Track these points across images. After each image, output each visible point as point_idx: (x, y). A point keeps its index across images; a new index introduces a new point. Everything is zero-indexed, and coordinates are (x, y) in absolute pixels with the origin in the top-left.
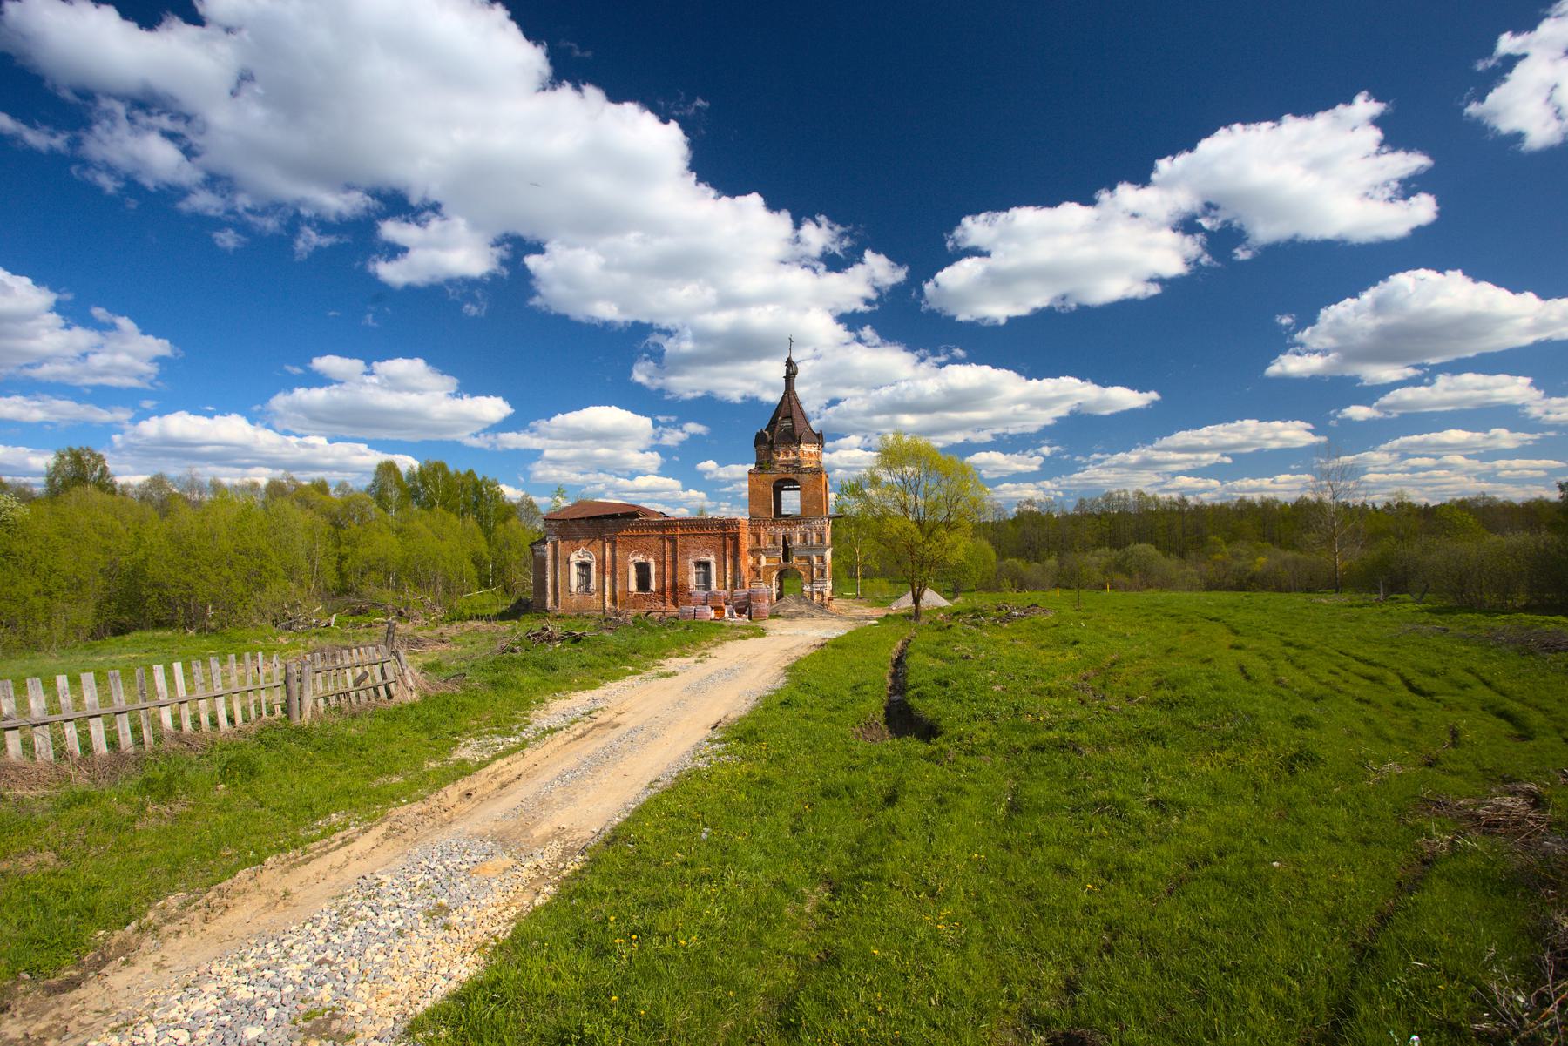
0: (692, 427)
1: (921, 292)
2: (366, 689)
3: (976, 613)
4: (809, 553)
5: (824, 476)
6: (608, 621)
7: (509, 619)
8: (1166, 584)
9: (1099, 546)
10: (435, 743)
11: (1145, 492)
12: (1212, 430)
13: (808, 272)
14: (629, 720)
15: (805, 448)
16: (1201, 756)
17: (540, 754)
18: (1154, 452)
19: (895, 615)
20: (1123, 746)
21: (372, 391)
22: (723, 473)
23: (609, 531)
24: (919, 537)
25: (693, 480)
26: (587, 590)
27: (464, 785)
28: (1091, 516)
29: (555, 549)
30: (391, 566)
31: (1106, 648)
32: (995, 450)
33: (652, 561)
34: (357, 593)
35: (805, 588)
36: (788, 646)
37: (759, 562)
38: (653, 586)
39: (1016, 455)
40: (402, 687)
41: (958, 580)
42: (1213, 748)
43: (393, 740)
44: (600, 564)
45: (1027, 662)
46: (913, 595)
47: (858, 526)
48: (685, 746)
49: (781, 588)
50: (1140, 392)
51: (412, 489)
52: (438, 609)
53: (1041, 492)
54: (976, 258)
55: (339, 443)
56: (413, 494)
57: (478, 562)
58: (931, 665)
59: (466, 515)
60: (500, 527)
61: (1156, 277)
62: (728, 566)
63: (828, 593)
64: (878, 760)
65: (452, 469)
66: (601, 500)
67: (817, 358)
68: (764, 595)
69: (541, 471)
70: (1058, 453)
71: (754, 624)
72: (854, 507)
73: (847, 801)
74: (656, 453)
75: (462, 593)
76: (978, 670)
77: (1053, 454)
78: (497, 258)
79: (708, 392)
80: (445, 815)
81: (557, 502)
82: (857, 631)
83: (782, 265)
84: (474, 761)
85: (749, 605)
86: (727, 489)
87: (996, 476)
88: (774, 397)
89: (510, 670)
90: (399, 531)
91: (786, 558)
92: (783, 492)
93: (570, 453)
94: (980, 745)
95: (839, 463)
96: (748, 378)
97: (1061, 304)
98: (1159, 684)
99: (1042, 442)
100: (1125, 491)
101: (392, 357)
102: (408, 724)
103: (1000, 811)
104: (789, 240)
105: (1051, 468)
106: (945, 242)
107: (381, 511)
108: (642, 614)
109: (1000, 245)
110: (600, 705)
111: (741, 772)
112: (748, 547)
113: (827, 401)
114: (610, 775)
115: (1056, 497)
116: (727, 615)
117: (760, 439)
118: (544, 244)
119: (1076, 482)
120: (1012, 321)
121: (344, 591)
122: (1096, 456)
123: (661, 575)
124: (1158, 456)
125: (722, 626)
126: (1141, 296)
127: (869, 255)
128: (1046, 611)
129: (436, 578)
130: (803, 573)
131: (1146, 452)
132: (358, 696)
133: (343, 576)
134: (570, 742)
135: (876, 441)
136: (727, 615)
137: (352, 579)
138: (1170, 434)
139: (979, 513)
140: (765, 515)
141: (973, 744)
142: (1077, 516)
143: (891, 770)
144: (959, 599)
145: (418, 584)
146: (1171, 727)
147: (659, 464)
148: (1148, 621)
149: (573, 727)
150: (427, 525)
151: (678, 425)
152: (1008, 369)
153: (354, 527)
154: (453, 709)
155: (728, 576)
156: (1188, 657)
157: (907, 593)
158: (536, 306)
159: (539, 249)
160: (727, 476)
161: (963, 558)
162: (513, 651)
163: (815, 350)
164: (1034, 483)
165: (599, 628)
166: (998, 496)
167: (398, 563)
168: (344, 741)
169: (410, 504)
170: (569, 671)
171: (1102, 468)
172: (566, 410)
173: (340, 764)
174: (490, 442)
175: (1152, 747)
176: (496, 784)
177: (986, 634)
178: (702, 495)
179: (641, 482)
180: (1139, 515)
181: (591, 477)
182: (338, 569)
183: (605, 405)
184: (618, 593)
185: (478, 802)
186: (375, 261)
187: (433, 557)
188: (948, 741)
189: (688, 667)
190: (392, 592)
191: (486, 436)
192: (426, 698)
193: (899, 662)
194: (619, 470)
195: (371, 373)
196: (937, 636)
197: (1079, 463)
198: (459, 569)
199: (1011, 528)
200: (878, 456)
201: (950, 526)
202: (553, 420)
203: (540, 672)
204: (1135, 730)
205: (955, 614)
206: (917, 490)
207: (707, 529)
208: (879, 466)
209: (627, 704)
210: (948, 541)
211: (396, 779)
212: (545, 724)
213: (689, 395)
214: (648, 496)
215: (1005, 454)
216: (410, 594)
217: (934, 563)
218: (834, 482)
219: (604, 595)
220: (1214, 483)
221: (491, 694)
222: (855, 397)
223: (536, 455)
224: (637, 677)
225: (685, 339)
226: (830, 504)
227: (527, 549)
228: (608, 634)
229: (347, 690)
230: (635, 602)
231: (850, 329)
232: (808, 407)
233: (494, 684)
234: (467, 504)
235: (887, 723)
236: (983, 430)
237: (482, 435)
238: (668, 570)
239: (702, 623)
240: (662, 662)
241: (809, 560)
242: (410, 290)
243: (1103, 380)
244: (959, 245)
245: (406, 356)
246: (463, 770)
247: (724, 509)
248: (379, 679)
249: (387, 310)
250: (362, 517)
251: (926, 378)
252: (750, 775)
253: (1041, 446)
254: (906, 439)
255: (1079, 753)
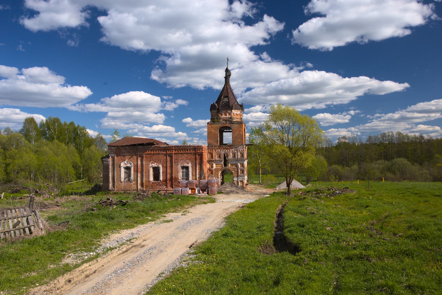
0: (180, 102)
1: (291, 35)
2: (19, 229)
3: (318, 192)
4: (236, 162)
5: (244, 125)
6: (139, 195)
7: (91, 195)
8: (413, 178)
9: (379, 159)
10: (53, 255)
11: (402, 132)
12: (436, 102)
13: (236, 26)
14: (149, 244)
15: (235, 112)
16: (431, 264)
17: (105, 260)
18: (407, 113)
19: (278, 192)
20: (391, 258)
21: (22, 83)
22: (195, 124)
23: (140, 152)
24: (289, 155)
25: (180, 127)
26: (129, 180)
27: (67, 276)
28: (375, 144)
29: (113, 160)
30: (32, 168)
31: (383, 209)
32: (327, 112)
33: (161, 166)
34: (15, 182)
35: (234, 179)
36: (226, 207)
37: (212, 167)
38: (161, 178)
39: (337, 115)
40: (37, 228)
41: (309, 176)
42: (438, 260)
43: (33, 254)
44: (136, 167)
45: (343, 216)
46: (287, 183)
47: (260, 149)
48: (177, 256)
49: (223, 179)
50: (400, 83)
51: (42, 131)
52: (55, 190)
53: (350, 133)
54: (318, 18)
55: (5, 108)
56: (43, 134)
57: (75, 167)
58: (295, 217)
59: (69, 143)
60: (87, 150)
61: (408, 26)
62: (197, 169)
63: (245, 182)
64: (270, 263)
65: (62, 122)
66: (136, 137)
67: (241, 68)
68: (214, 182)
69: (106, 123)
70: (358, 114)
71: (210, 197)
72: (258, 140)
73: (255, 283)
74: (162, 114)
75: (67, 182)
76: (319, 220)
77: (356, 115)
78: (84, 17)
79: (187, 84)
80: (58, 291)
81: (115, 137)
82: (260, 200)
83: (223, 22)
84: (72, 264)
85: (207, 187)
86: (197, 132)
87: (327, 125)
88: (219, 87)
89: (91, 219)
90: (36, 152)
91: (225, 164)
92: (224, 133)
93: (121, 114)
94: (320, 256)
95: (251, 119)
96: (207, 78)
97: (360, 40)
98: (409, 228)
99: (350, 108)
100: (392, 132)
101: (32, 66)
102: (40, 246)
103: (331, 289)
104: (227, 10)
105: (354, 122)
106: (303, 10)
107: (27, 142)
108: (156, 192)
109: (331, 11)
110: (135, 236)
111: (204, 269)
112: (207, 159)
113: (245, 89)
114: (139, 271)
115: (357, 135)
116: (197, 192)
117: (213, 107)
118: (107, 11)
119: (367, 128)
120: (335, 48)
121: (8, 181)
122: (378, 115)
123: (165, 173)
124: (409, 115)
125: (194, 198)
126: (401, 36)
127: (266, 17)
128: (352, 191)
129: (54, 175)
130: (234, 172)
131: (403, 113)
132: (15, 233)
133: (7, 174)
134: (120, 254)
135: (269, 108)
136: (197, 192)
137: (12, 175)
138: (415, 104)
139: (319, 143)
140: (215, 144)
141: (317, 256)
142: (368, 144)
143: (276, 268)
144: (309, 185)
145: (46, 178)
146: (416, 249)
147: (164, 119)
148: (403, 196)
149: (122, 247)
150: (50, 149)
151: (173, 100)
152: (334, 73)
153: (13, 150)
154: (62, 239)
155: (197, 173)
156: (424, 214)
157: (284, 182)
158: (104, 42)
159: (105, 13)
160: (197, 125)
161: (311, 165)
162: (92, 210)
163: (239, 64)
164: (346, 128)
165: (135, 198)
166: (329, 135)
167: (36, 168)
168: (8, 255)
169: (42, 139)
170: (120, 220)
171: (381, 121)
172: (119, 92)
173: (5, 267)
174: (81, 108)
175: (406, 259)
176: (83, 276)
177: (322, 202)
178: (185, 134)
179: (156, 128)
180: (399, 144)
181: (131, 125)
182: (6, 170)
183: (138, 91)
184: (144, 181)
185: (74, 285)
186: (23, 19)
187: (53, 164)
188: (304, 254)
189: (178, 217)
190: (32, 182)
191: (79, 105)
192: (49, 233)
193: (280, 215)
194: (145, 122)
195: (22, 74)
196: (299, 203)
197: (369, 119)
198: (66, 170)
199: (334, 150)
200: (269, 116)
201: (305, 149)
202: (112, 98)
203: (106, 220)
204: (398, 250)
205: (307, 192)
206: (288, 132)
207: (187, 151)
208: (270, 120)
209: (148, 236)
210: (304, 156)
211: (33, 274)
212: (108, 246)
213: (179, 86)
214: (159, 135)
215: (332, 114)
216: (41, 183)
217: (297, 167)
218: (249, 128)
219: (137, 183)
220: (437, 128)
221: (82, 231)
222: (259, 87)
223: (104, 115)
224: (153, 223)
225: (177, 58)
226: (246, 139)
227: (100, 160)
228: (138, 201)
229: (9, 230)
230: (152, 186)
231: (256, 54)
232: (236, 92)
233: (83, 226)
234: (70, 139)
235: (274, 245)
236: (321, 103)
237: (77, 105)
238: (169, 170)
239: (185, 196)
240: (165, 215)
241: (237, 166)
242: (40, 33)
243: (381, 78)
244: (311, 11)
245: (38, 66)
246: (67, 269)
247: (196, 141)
248: (26, 224)
249: (29, 43)
250: (18, 145)
251: (293, 77)
252: (208, 270)
253: (351, 110)
254: (283, 107)
255: (370, 261)
